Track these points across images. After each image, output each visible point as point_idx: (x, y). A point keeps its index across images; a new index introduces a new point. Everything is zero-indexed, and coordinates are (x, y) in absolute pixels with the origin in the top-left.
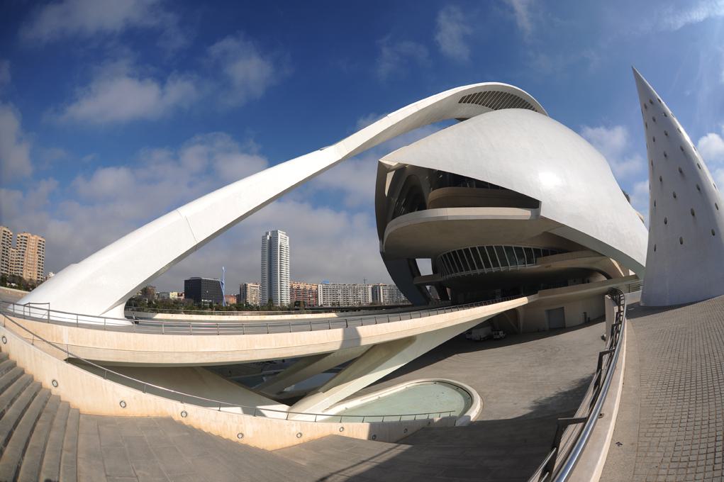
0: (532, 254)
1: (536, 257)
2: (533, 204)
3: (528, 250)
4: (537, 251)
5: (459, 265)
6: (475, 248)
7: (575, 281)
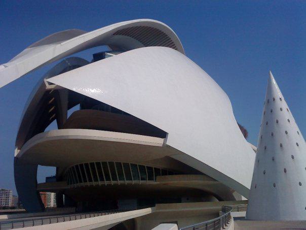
0: (152, 172)
1: (156, 176)
2: (162, 134)
3: (150, 168)
4: (157, 170)
5: (99, 168)
6: (99, 163)
7: (188, 199)
